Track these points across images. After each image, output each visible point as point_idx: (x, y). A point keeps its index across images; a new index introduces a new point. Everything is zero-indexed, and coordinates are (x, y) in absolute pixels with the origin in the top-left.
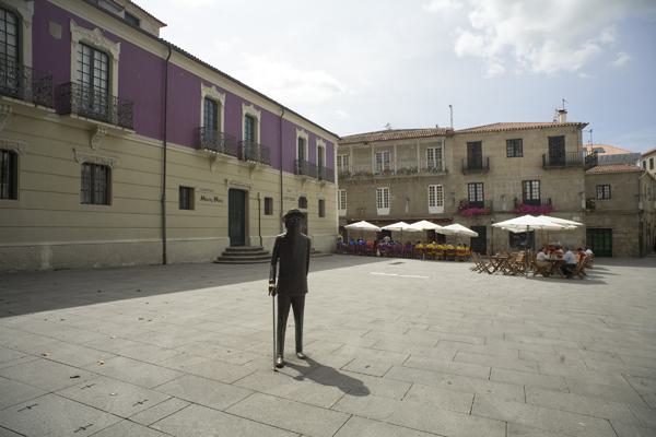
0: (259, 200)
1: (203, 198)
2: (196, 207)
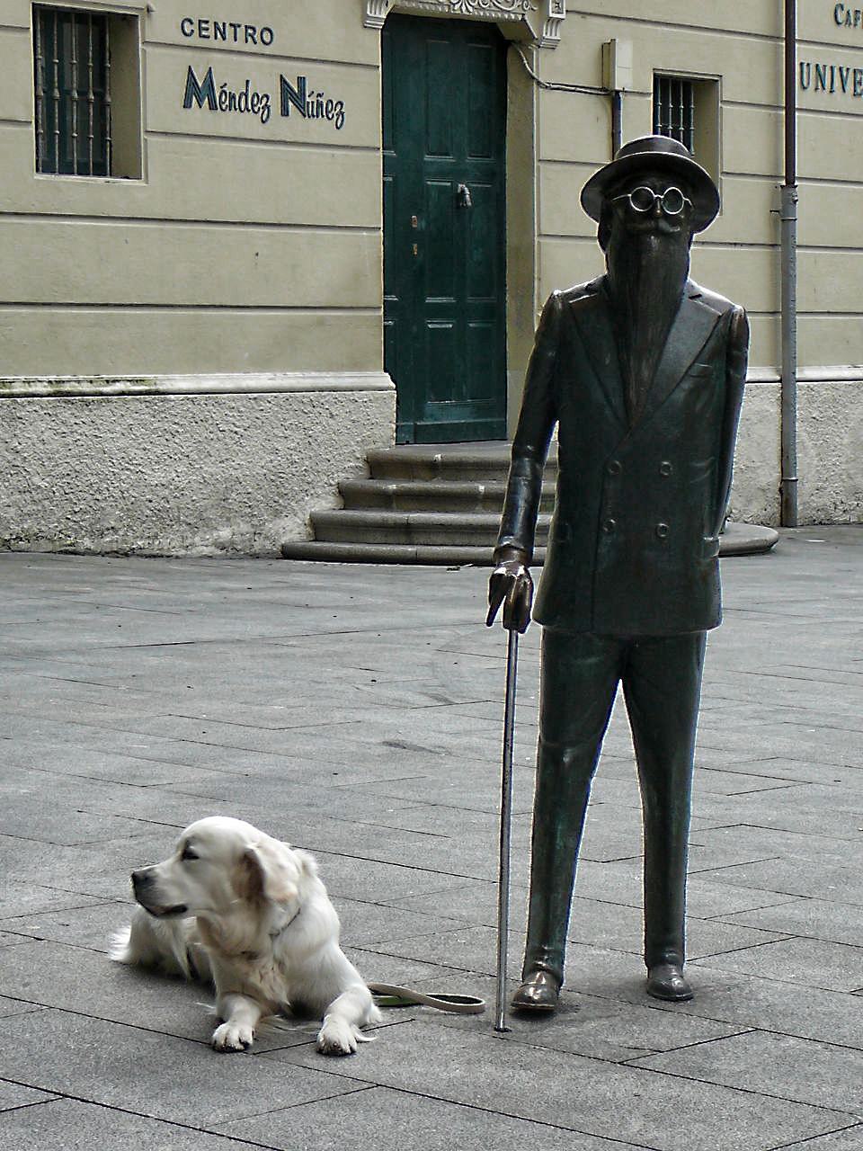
0: (613, 99)
1: (199, 91)
2: (155, 151)
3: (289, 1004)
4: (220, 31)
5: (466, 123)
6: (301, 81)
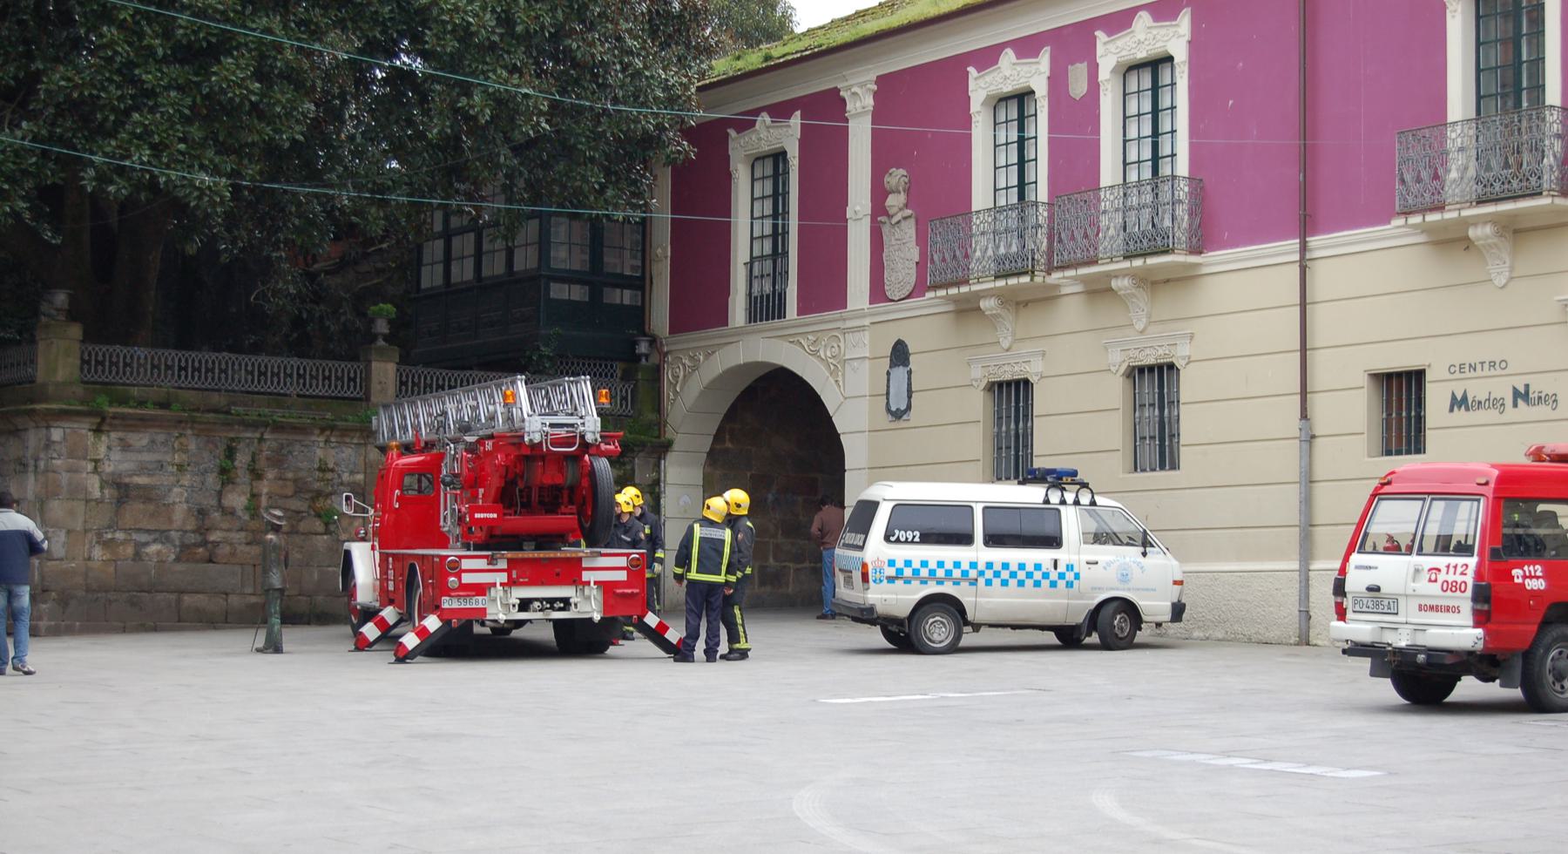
3: (1407, 702)
4: (1473, 367)
5: (54, 242)
6: (1527, 386)
